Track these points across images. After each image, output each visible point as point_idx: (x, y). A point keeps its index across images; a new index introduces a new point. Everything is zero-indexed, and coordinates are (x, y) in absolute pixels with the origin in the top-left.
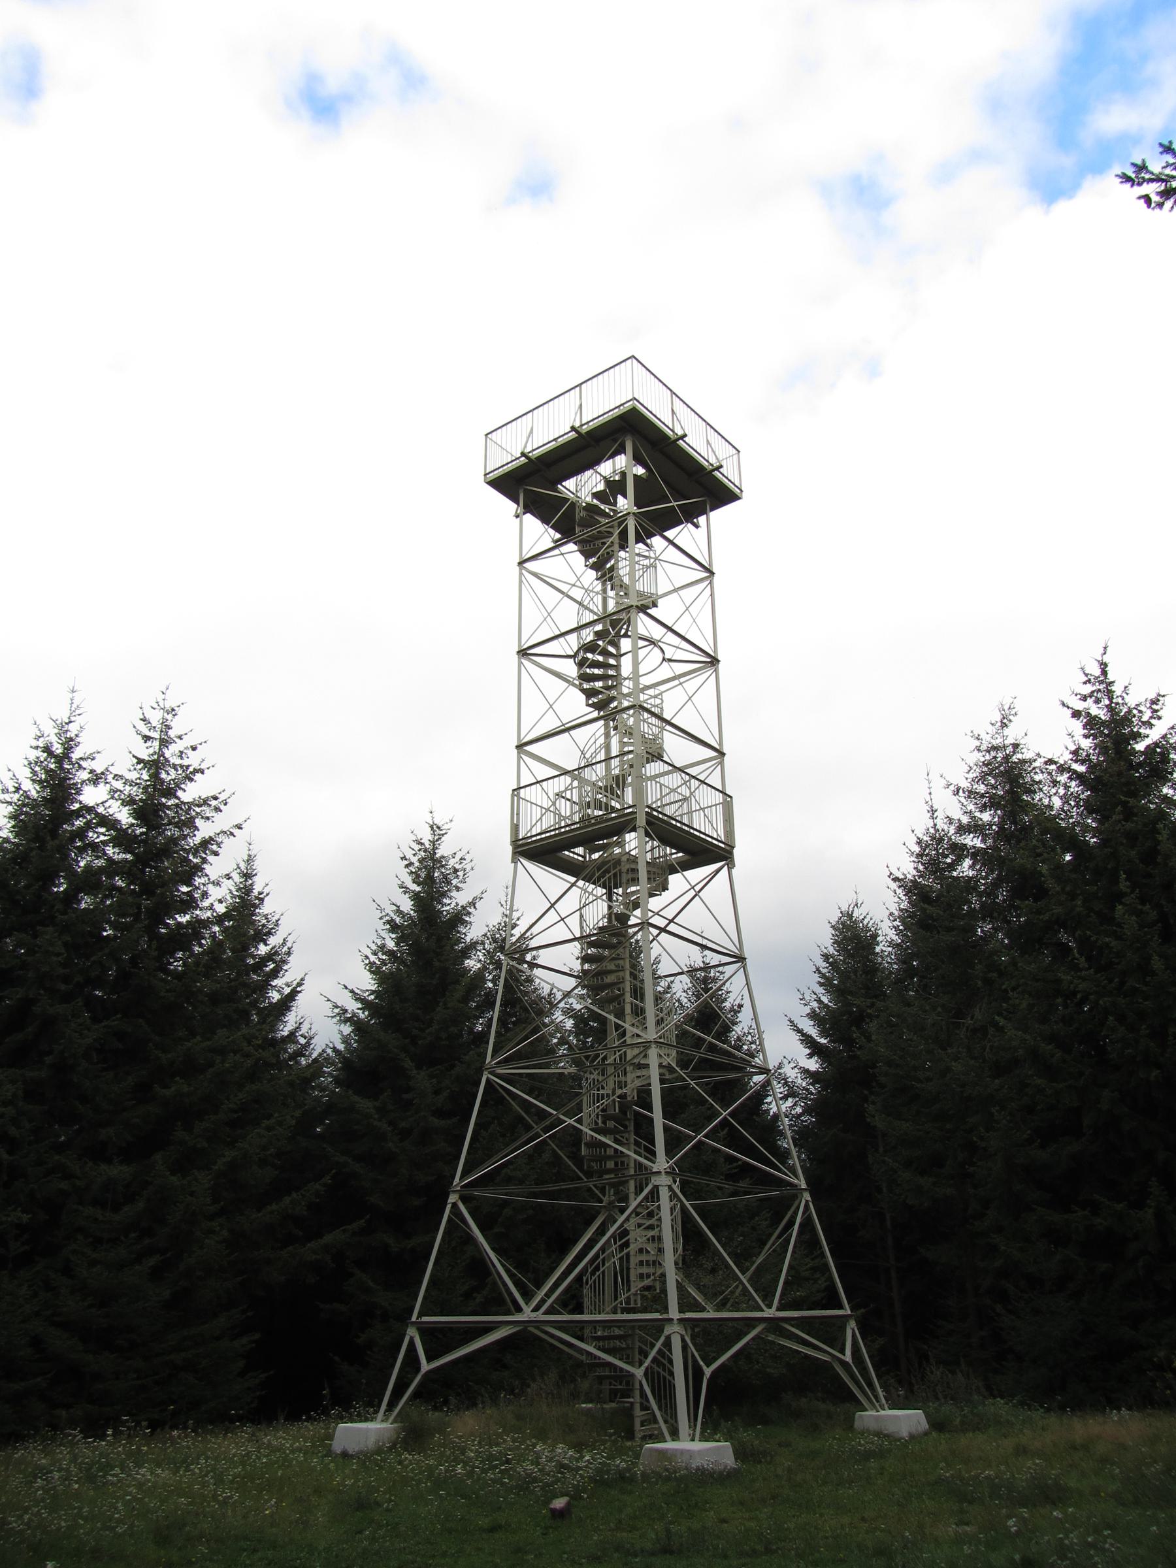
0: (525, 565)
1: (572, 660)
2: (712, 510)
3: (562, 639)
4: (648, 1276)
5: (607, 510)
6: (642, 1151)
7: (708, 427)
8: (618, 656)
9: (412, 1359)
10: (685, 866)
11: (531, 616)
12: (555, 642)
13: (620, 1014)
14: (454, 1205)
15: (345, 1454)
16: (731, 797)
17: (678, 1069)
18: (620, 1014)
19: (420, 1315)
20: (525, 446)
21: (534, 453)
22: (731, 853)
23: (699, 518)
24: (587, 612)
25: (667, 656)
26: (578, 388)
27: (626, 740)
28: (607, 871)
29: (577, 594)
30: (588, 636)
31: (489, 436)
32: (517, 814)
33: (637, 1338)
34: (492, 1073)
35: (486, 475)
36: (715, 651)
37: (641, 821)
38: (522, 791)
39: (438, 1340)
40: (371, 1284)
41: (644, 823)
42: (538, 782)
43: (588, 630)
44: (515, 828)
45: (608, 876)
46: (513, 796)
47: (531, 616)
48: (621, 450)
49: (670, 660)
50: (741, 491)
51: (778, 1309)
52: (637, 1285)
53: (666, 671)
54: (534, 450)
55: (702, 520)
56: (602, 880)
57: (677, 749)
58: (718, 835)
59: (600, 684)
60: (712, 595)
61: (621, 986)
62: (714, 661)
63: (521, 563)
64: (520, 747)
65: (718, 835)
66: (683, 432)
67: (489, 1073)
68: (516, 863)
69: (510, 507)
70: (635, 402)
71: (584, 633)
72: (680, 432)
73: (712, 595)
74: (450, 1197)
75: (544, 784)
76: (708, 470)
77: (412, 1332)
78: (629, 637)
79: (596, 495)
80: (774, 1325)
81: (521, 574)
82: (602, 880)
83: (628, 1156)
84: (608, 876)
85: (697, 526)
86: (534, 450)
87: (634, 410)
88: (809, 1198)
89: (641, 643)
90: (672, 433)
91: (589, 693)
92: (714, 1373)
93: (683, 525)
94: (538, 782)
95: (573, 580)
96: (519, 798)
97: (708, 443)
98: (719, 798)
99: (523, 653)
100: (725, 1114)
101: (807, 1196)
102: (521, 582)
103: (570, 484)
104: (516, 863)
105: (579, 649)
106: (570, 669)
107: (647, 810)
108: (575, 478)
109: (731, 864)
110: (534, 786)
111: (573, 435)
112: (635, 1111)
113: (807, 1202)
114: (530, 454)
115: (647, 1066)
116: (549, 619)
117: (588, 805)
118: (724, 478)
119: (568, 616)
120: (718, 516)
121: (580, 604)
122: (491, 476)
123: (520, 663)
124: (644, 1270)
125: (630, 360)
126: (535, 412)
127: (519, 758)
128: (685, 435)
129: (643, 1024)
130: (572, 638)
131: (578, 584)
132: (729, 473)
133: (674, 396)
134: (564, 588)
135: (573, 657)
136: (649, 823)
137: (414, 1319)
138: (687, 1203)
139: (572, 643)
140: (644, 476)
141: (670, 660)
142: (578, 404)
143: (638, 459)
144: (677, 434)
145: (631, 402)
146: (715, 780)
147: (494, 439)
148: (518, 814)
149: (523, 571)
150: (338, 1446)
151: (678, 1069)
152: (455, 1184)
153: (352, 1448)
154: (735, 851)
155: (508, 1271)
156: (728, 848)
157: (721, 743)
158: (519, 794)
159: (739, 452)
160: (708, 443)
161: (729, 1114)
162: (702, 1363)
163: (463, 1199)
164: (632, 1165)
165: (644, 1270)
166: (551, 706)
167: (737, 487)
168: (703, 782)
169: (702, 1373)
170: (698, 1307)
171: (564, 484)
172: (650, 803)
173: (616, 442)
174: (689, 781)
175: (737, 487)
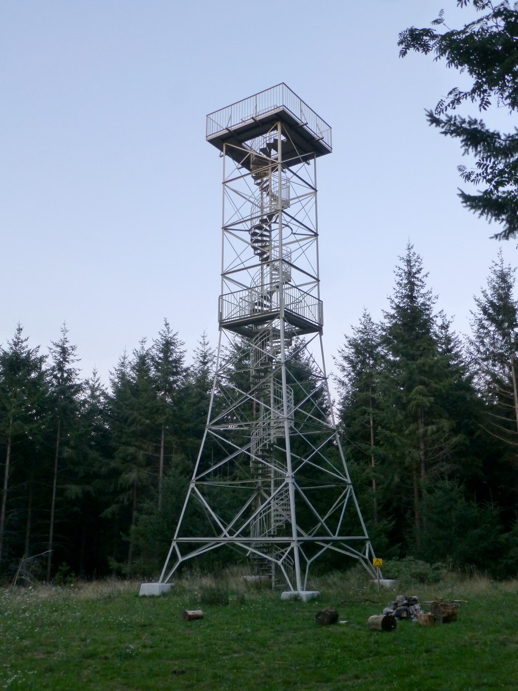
0: (226, 184)
1: (248, 232)
2: (318, 156)
3: (244, 223)
4: (280, 521)
5: (263, 154)
6: (277, 465)
7: (317, 117)
8: (270, 231)
9: (174, 555)
10: (300, 333)
11: (229, 212)
12: (241, 224)
13: (268, 403)
14: (193, 489)
15: (144, 596)
16: (322, 302)
17: (295, 429)
18: (268, 403)
19: (178, 537)
20: (228, 126)
21: (232, 128)
22: (322, 328)
23: (310, 161)
24: (256, 207)
25: (293, 232)
26: (255, 97)
27: (274, 272)
28: (265, 336)
29: (252, 200)
30: (257, 222)
31: (209, 116)
32: (222, 308)
33: (274, 548)
34: (210, 429)
35: (207, 136)
36: (317, 230)
37: (283, 315)
38: (224, 297)
39: (186, 548)
40: (493, 424)
41: (283, 316)
42: (232, 293)
43: (256, 219)
44: (221, 314)
45: (264, 339)
46: (219, 298)
47: (229, 212)
48: (276, 128)
49: (295, 234)
50: (332, 149)
51: (338, 536)
52: (273, 525)
53: (292, 238)
54: (232, 126)
55: (312, 161)
56: (262, 341)
57: (297, 277)
58: (316, 320)
59: (260, 244)
60: (316, 202)
61: (269, 389)
62: (316, 235)
63: (224, 183)
64: (223, 275)
65: (316, 320)
66: (306, 122)
67: (208, 429)
68: (221, 331)
69: (218, 151)
70: (284, 107)
71: (254, 220)
72: (305, 122)
73: (316, 202)
74: (191, 485)
75: (235, 294)
76: (317, 139)
77: (174, 544)
78: (278, 223)
79: (261, 150)
80: (335, 543)
81: (224, 189)
82: (262, 341)
83: (271, 467)
84: (264, 339)
85: (308, 164)
86: (232, 126)
87: (283, 111)
88: (352, 488)
89: (283, 226)
90: (300, 122)
91: (255, 249)
92: (312, 563)
93: (301, 164)
94: (232, 293)
95: (250, 194)
96: (223, 300)
97: (317, 125)
98: (317, 301)
99: (225, 229)
100: (317, 450)
101: (351, 487)
102: (224, 193)
103: (248, 143)
104: (221, 331)
105: (251, 228)
106: (247, 237)
107: (285, 310)
108: (250, 141)
109: (321, 334)
110: (230, 295)
111: (252, 121)
112: (275, 448)
113: (351, 489)
114: (230, 129)
115: (283, 427)
116: (238, 213)
117: (256, 304)
118: (323, 143)
119: (247, 210)
120: (319, 159)
121: (253, 203)
122: (210, 138)
123: (223, 234)
124: (278, 518)
125: (282, 85)
126: (233, 106)
127: (223, 280)
128: (307, 123)
129: (280, 408)
130: (249, 223)
131: (253, 196)
132: (326, 141)
133: (302, 102)
134: (247, 197)
135: (249, 231)
136: (285, 315)
137: (175, 538)
138: (299, 489)
139: (248, 225)
140: (285, 141)
141: (295, 234)
142: (255, 106)
143: (283, 133)
144: (303, 123)
145: (282, 107)
146: (314, 293)
147: (211, 118)
148: (222, 308)
149: (226, 187)
150: (141, 593)
151: (295, 429)
152: (192, 479)
153: (147, 594)
154: (323, 327)
155: (218, 518)
156: (320, 326)
157: (318, 275)
158: (222, 298)
159: (331, 128)
160: (317, 125)
161: (319, 450)
162: (306, 559)
163: (197, 486)
164: (272, 471)
165: (278, 518)
166: (238, 256)
167: (327, 144)
168: (308, 294)
169: (306, 563)
170: (302, 536)
171: (246, 142)
172: (292, 308)
173: (273, 125)
174: (304, 294)
175: (327, 144)
